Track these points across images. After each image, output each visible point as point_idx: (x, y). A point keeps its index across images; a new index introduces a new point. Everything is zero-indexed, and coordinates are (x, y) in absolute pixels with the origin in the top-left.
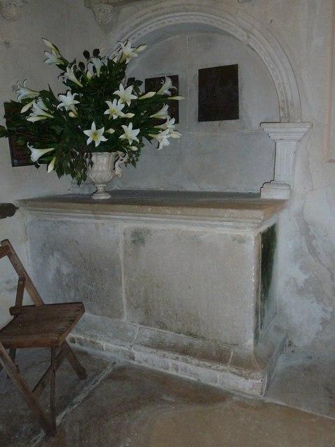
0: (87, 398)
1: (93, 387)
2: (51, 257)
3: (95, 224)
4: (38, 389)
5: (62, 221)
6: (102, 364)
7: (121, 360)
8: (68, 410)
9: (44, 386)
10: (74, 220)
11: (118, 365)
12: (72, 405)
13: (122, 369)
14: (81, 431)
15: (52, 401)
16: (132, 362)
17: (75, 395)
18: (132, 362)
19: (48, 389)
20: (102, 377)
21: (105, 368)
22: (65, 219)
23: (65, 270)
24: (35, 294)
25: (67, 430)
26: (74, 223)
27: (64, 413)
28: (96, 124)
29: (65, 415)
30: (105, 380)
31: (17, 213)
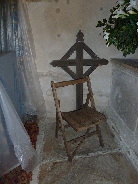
0: (95, 156)
1: (102, 153)
2: (117, 87)
3: (136, 79)
4: (72, 142)
5: (124, 73)
6: (115, 145)
7: (124, 151)
8: (84, 156)
9: (75, 142)
10: (128, 74)
11: (121, 151)
12: (88, 155)
13: (121, 155)
14: (79, 169)
15: (77, 148)
16: (128, 155)
17: (93, 152)
18: (128, 155)
19: (78, 143)
20: (109, 152)
21: (115, 149)
22: (125, 72)
23: (120, 96)
24: (93, 104)
25: (76, 164)
26: (128, 75)
27: (82, 156)
28: (128, 16)
29: (82, 157)
30: (109, 154)
31: (108, 64)
